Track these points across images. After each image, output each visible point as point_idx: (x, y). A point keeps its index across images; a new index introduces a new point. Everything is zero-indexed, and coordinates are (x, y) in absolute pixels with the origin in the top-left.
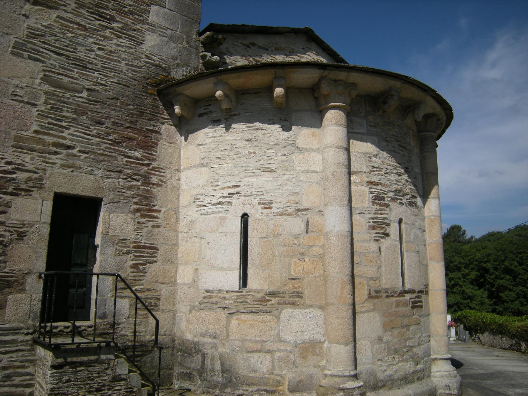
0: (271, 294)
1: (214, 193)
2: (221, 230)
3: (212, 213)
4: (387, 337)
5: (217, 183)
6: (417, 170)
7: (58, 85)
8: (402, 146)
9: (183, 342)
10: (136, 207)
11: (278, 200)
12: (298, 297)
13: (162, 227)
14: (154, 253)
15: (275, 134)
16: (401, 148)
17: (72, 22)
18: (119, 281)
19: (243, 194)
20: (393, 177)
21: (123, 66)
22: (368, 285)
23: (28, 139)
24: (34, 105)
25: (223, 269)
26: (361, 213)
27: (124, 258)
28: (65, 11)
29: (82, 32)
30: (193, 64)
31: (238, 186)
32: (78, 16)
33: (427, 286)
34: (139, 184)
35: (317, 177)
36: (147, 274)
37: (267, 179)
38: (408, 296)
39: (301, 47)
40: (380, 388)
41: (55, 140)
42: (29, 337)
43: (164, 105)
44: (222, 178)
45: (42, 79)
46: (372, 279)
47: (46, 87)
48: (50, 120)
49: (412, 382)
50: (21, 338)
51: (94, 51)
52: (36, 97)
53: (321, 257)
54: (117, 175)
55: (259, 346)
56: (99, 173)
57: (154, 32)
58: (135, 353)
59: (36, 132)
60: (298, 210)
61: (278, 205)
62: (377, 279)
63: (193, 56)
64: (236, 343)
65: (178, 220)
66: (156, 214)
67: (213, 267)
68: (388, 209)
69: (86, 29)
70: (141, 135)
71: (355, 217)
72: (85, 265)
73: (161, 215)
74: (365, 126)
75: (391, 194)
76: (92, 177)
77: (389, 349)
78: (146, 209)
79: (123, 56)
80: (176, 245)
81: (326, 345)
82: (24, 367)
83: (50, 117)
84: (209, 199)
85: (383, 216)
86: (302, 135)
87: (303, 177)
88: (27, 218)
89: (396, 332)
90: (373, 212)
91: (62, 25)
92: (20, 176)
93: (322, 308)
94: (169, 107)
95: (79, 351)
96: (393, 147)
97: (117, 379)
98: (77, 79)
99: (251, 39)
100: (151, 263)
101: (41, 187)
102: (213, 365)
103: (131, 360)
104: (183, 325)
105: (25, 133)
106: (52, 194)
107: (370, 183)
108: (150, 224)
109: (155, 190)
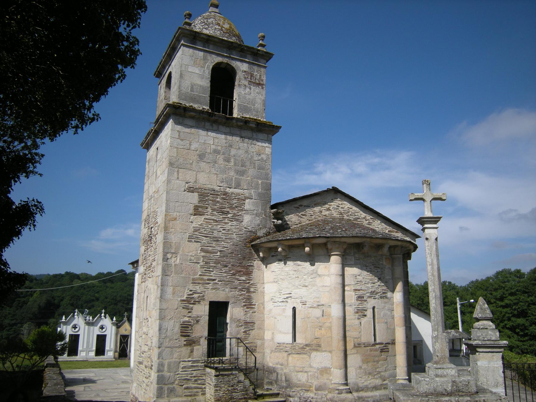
0: (307, 345)
1: (280, 296)
3: (279, 306)
4: (364, 366)
6: (388, 277)
7: (207, 252)
8: (376, 267)
9: (268, 367)
10: (244, 304)
12: (319, 347)
15: (308, 268)
17: (210, 220)
20: (369, 285)
21: (234, 236)
22: (354, 341)
23: (197, 279)
24: (198, 263)
25: (285, 333)
27: (240, 328)
28: (207, 215)
30: (268, 226)
33: (394, 340)
34: (245, 293)
35: (328, 289)
38: (378, 346)
40: (360, 391)
42: (203, 364)
43: (255, 251)
46: (356, 338)
47: (203, 254)
49: (380, 389)
50: (200, 364)
52: (199, 259)
53: (330, 328)
54: (235, 290)
55: (301, 369)
56: (227, 290)
58: (247, 371)
59: (200, 275)
60: (319, 305)
61: (309, 303)
62: (359, 338)
63: (268, 222)
64: (292, 368)
65: (264, 308)
67: (280, 332)
69: (216, 221)
71: (347, 308)
72: (222, 332)
73: (256, 307)
75: (368, 295)
77: (366, 373)
78: (249, 304)
80: (264, 320)
81: (332, 369)
82: (202, 377)
86: (320, 267)
88: (200, 314)
89: (370, 364)
91: (207, 222)
92: (196, 296)
93: (330, 352)
94: (257, 252)
95: (224, 370)
97: (239, 382)
99: (299, 203)
100: (252, 330)
101: (204, 300)
102: (281, 378)
103: (245, 374)
104: (268, 359)
107: (355, 290)
108: (251, 311)
109: (252, 295)
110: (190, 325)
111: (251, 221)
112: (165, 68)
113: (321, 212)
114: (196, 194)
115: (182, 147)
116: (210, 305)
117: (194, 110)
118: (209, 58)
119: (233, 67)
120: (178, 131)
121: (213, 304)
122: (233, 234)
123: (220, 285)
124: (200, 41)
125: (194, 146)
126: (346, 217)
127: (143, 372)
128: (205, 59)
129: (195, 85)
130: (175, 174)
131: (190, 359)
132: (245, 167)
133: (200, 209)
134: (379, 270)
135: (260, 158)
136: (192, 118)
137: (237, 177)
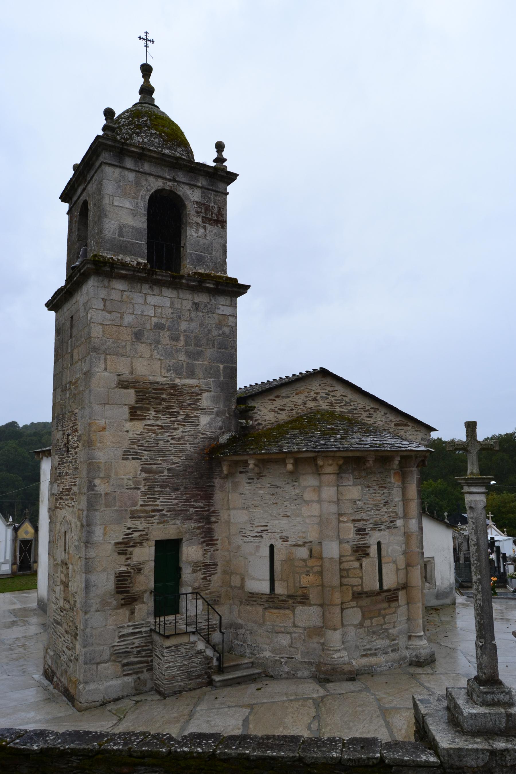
1: (251, 529)
2: (257, 554)
3: (251, 542)
5: (253, 523)
8: (382, 487)
10: (202, 540)
11: (292, 536)
13: (219, 550)
14: (216, 567)
16: (381, 489)
17: (153, 426)
18: (199, 599)
19: (270, 531)
21: (188, 447)
22: (352, 590)
24: (138, 489)
26: (348, 542)
28: (149, 419)
29: (161, 431)
31: (267, 526)
32: (157, 420)
36: (212, 582)
37: (285, 522)
39: (318, 385)
41: (152, 508)
44: (256, 519)
45: (141, 470)
47: (144, 475)
48: (148, 496)
51: (168, 442)
57: (205, 413)
59: (141, 505)
60: (305, 543)
61: (292, 540)
66: (215, 542)
67: (253, 578)
68: (368, 536)
69: (161, 427)
70: (202, 491)
73: (218, 542)
74: (352, 479)
75: (371, 526)
76: (175, 526)
78: (208, 539)
79: (186, 439)
83: (148, 494)
84: (249, 532)
85: (364, 542)
87: (308, 520)
88: (142, 559)
90: (357, 540)
91: (148, 429)
92: (136, 535)
96: (374, 490)
98: (161, 464)
100: (214, 574)
105: (136, 508)
106: (154, 542)
107: (354, 520)
108: (212, 549)
109: (215, 526)
110: (129, 576)
111: (210, 424)
112: (76, 190)
113: (305, 404)
114: (132, 391)
115: (109, 323)
116: (156, 546)
117: (125, 265)
118: (144, 183)
119: (179, 196)
120: (103, 299)
121: (160, 545)
122: (185, 444)
123: (169, 517)
124: (129, 156)
125: (128, 319)
126: (338, 409)
127: (63, 638)
128: (138, 183)
129: (124, 226)
130: (102, 363)
131: (130, 624)
132: (201, 346)
133: (139, 412)
134: (385, 491)
135: (221, 332)
136: (123, 277)
137: (190, 361)
